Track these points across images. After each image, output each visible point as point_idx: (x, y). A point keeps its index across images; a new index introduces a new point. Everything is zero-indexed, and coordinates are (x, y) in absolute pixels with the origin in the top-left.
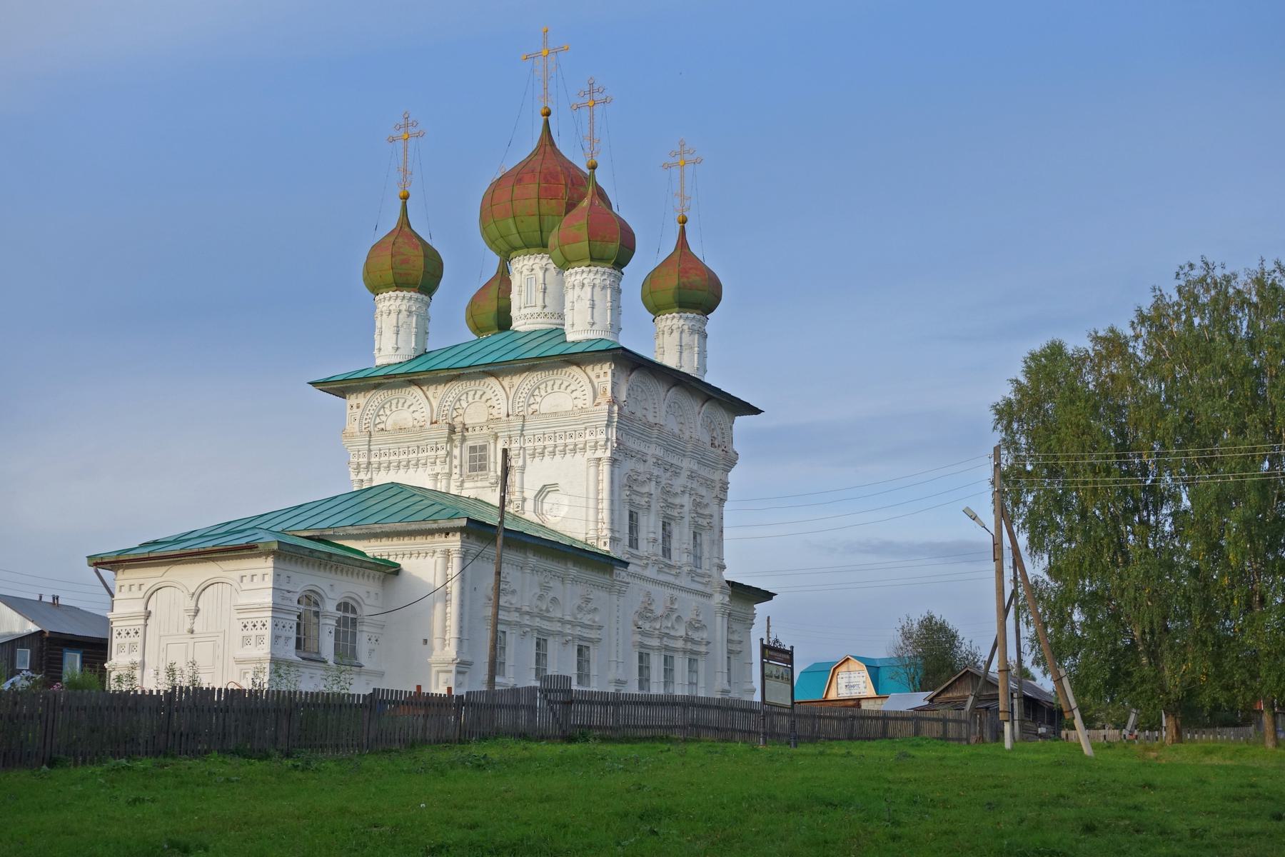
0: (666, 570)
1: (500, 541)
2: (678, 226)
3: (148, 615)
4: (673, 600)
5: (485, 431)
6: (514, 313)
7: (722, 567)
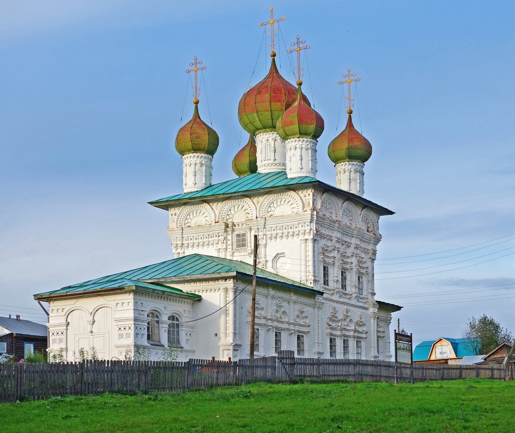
0: (344, 296)
2: (348, 115)
3: (68, 324)
4: (347, 311)
5: (244, 226)
6: (258, 164)
7: (374, 294)
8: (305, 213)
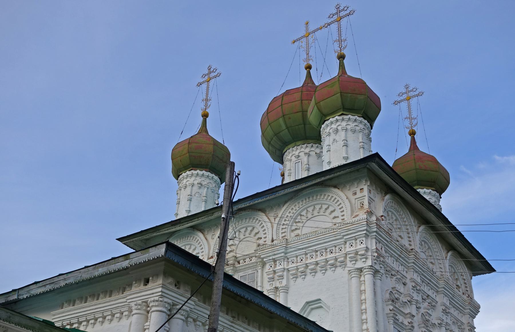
1: (217, 295)
2: (409, 138)
8: (356, 219)
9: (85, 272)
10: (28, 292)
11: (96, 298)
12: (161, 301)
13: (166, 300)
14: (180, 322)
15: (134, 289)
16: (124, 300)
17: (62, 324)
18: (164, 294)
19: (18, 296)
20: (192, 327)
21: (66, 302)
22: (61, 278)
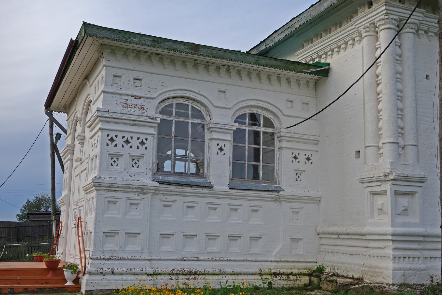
9: (313, 10)
10: (272, 40)
11: (329, 32)
12: (387, 19)
13: (392, 17)
14: (411, 35)
15: (360, 15)
16: (353, 27)
17: (306, 61)
18: (389, 12)
19: (266, 46)
20: (424, 38)
21: (305, 42)
22: (295, 21)
